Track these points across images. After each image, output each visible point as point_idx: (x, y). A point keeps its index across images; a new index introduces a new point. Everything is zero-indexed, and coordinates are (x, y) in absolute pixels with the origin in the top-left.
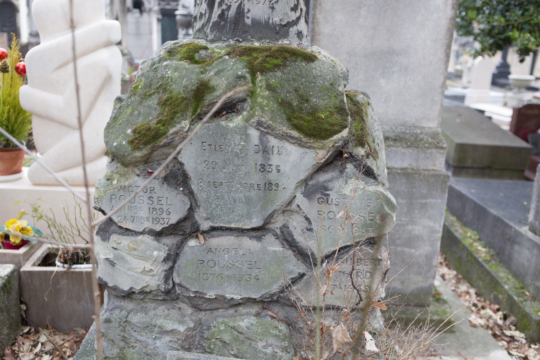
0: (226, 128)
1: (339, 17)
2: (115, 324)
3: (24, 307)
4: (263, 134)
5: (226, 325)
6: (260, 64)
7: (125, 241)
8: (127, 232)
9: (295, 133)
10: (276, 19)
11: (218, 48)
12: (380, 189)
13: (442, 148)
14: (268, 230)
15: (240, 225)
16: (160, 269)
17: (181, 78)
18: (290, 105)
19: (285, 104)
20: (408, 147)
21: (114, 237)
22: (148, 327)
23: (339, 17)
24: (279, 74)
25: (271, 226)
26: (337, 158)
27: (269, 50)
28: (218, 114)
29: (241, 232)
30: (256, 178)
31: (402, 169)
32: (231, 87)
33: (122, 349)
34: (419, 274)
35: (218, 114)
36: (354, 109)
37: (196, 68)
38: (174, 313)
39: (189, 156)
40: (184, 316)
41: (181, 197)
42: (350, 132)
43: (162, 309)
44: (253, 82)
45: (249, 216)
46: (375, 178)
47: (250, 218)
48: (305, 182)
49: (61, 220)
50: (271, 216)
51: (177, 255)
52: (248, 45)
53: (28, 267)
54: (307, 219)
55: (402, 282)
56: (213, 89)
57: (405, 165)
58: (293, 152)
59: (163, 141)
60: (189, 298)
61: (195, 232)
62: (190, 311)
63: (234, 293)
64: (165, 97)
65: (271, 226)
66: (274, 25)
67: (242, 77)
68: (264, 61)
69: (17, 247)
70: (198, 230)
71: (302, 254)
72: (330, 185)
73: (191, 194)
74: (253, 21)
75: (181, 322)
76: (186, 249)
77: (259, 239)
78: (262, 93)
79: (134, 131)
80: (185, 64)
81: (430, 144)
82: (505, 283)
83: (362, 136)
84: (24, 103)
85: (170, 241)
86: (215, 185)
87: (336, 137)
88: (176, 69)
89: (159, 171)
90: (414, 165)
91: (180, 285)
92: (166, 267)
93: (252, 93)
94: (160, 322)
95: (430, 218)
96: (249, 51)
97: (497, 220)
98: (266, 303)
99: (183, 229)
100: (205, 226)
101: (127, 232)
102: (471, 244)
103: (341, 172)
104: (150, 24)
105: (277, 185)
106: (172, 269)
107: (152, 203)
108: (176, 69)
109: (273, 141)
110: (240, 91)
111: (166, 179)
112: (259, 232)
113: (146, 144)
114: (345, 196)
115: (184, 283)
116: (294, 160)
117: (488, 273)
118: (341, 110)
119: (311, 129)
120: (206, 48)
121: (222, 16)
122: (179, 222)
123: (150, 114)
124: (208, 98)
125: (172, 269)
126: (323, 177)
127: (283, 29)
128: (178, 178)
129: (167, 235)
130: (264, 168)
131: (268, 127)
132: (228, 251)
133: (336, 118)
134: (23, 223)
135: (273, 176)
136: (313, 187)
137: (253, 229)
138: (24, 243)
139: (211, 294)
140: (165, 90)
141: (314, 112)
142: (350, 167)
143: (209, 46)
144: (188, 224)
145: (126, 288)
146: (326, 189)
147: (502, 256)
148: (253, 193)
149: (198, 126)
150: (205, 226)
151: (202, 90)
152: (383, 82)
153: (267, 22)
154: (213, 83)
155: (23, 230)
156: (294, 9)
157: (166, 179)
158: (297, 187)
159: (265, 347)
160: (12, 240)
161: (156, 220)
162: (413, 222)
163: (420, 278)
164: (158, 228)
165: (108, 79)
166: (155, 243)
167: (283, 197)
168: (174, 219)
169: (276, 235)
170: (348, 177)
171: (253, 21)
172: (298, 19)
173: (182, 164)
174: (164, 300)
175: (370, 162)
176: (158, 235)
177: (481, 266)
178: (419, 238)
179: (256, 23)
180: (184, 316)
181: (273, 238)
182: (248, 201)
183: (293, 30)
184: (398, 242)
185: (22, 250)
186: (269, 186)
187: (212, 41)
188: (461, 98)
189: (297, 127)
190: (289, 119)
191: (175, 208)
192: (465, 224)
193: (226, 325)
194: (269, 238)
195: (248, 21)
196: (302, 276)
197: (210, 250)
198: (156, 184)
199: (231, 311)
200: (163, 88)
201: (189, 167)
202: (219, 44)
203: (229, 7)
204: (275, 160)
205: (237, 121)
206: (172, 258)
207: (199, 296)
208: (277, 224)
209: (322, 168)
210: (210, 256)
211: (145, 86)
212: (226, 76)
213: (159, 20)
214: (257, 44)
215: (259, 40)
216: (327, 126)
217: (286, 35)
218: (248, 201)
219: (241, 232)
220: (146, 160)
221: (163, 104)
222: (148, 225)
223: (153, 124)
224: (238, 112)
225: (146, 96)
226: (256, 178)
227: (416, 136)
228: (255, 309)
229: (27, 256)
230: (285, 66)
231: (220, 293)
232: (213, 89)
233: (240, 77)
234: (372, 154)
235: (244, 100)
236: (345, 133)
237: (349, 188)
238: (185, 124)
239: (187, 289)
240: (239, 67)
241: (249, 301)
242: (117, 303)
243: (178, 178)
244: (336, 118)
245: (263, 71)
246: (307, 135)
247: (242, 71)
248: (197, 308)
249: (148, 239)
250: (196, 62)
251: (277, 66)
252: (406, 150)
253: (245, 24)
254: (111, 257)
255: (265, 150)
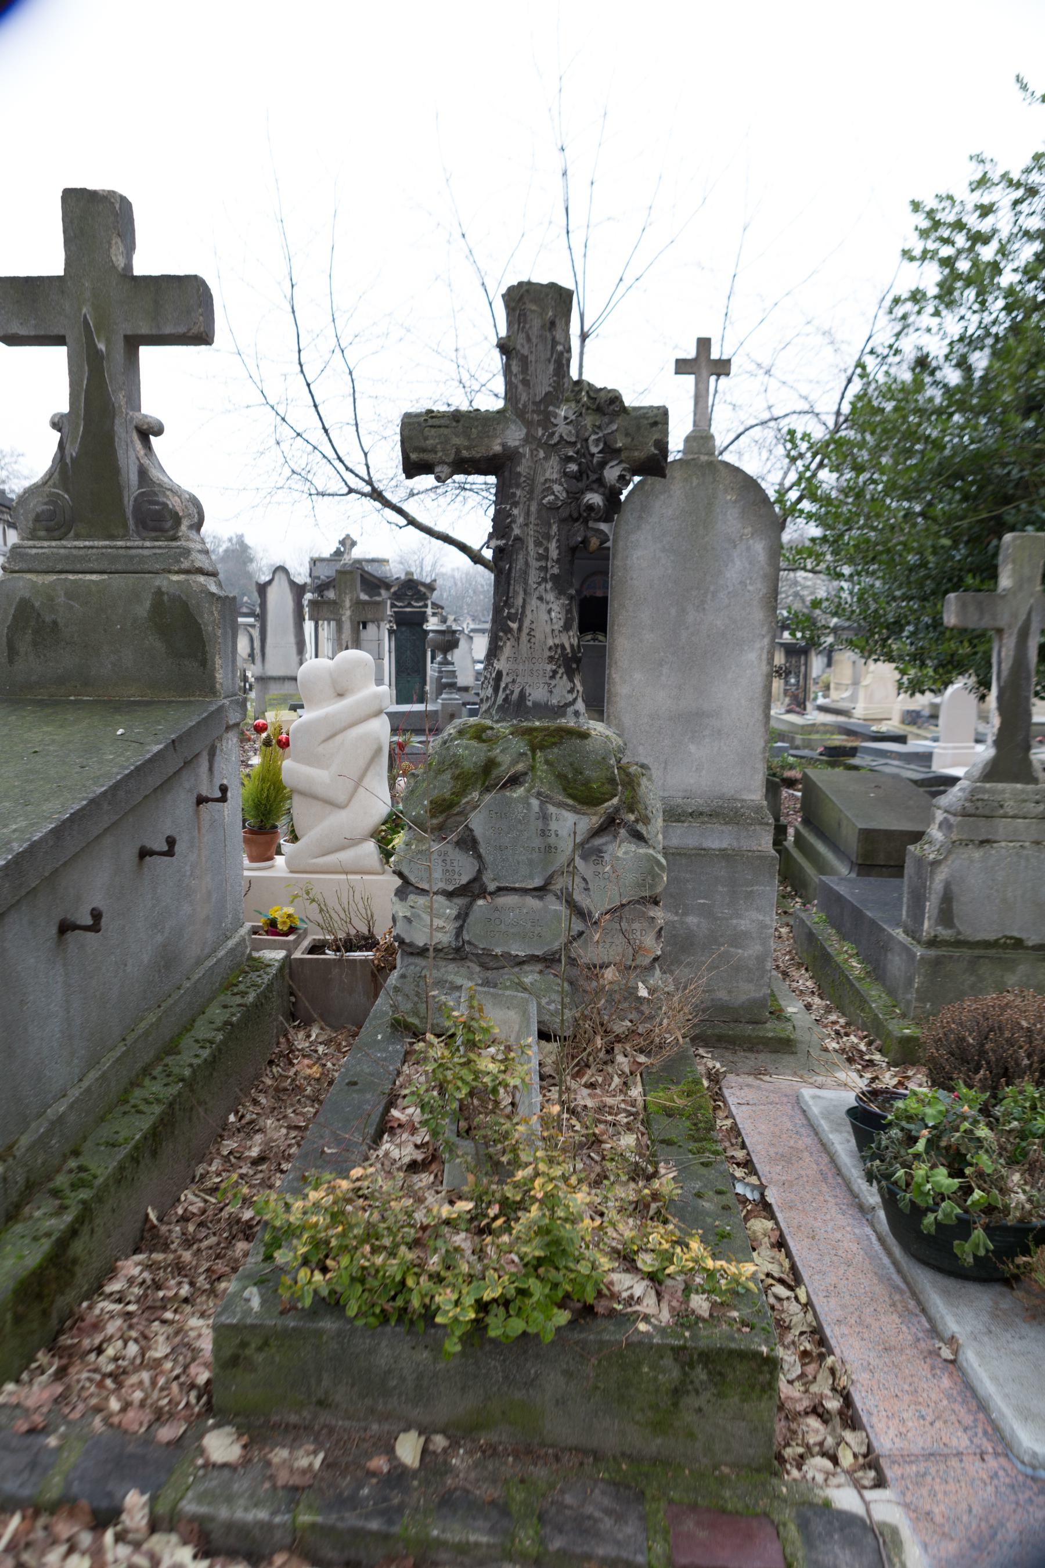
0: (511, 798)
1: (638, 676)
2: (410, 979)
3: (293, 999)
4: (542, 803)
5: (512, 981)
6: (539, 742)
7: (422, 901)
8: (423, 892)
9: (570, 802)
10: (554, 702)
11: (503, 728)
12: (651, 851)
13: (767, 824)
14: (550, 891)
15: (523, 885)
16: (451, 927)
17: (471, 755)
18: (566, 776)
19: (561, 777)
20: (726, 823)
21: (412, 897)
22: (439, 983)
23: (638, 676)
24: (556, 750)
25: (552, 887)
26: (609, 825)
27: (546, 729)
28: (504, 786)
29: (525, 891)
30: (537, 842)
31: (720, 850)
32: (514, 762)
33: (415, 1004)
34: (751, 981)
35: (504, 786)
36: (627, 779)
37: (484, 746)
38: (463, 970)
39: (478, 823)
40: (472, 973)
41: (471, 859)
42: (620, 800)
43: (452, 967)
44: (534, 759)
45: (531, 877)
46: (646, 842)
47: (533, 879)
48: (582, 844)
49: (332, 903)
50: (551, 877)
51: (467, 915)
52: (530, 724)
53: (297, 955)
54: (584, 879)
55: (729, 992)
56: (499, 765)
57: (724, 845)
58: (568, 819)
59: (457, 810)
60: (477, 955)
61: (483, 893)
62: (478, 969)
63: (519, 950)
64: (458, 772)
65: (552, 887)
66: (553, 707)
67: (524, 754)
68: (543, 740)
69: (286, 934)
70: (485, 891)
71: (581, 913)
72: (605, 848)
73: (479, 857)
74: (534, 703)
75: (470, 979)
76: (475, 907)
77: (541, 898)
78: (541, 767)
79: (431, 802)
80: (474, 743)
81: (752, 819)
82: (875, 1001)
83: (632, 804)
84: (285, 777)
85: (460, 901)
86: (501, 849)
87: (609, 803)
88: (466, 748)
89: (453, 837)
90: (735, 844)
91: (469, 943)
92: (457, 925)
93: (532, 768)
94: (450, 978)
95: (758, 910)
96: (530, 731)
97: (873, 923)
98: (549, 960)
99: (470, 891)
100: (492, 887)
101: (423, 892)
102: (846, 960)
103: (615, 837)
104: (380, 640)
105: (556, 848)
106: (461, 927)
107: (444, 865)
108: (466, 748)
109: (552, 809)
110: (520, 767)
111: (458, 844)
112: (541, 891)
113: (441, 812)
114: (618, 858)
115: (473, 941)
116: (569, 824)
117: (858, 992)
118: (612, 781)
119: (582, 794)
120: (492, 728)
121: (506, 700)
122: (469, 883)
123: (444, 786)
124: (495, 773)
125: (461, 927)
126: (598, 842)
127: (560, 710)
128: (468, 843)
129: (459, 896)
130: (544, 833)
131: (547, 796)
132: (513, 909)
133: (607, 788)
134: (290, 910)
135: (552, 840)
136: (589, 849)
137: (535, 889)
138: (292, 930)
139: (498, 951)
140: (457, 766)
141: (587, 783)
142: (623, 832)
143: (495, 726)
144: (476, 885)
145: (421, 944)
146: (601, 851)
147: (877, 971)
148: (535, 856)
149: (488, 797)
150: (492, 887)
151: (490, 765)
152: (692, 748)
153: (546, 704)
154: (499, 759)
155: (289, 916)
156: (571, 691)
157: (458, 844)
158: (574, 851)
159: (548, 1003)
160: (280, 927)
161: (449, 881)
162: (739, 916)
163: (751, 987)
164: (451, 888)
165: (379, 751)
166: (447, 903)
167: (562, 859)
168: (464, 880)
169: (556, 895)
170: (622, 842)
171: (534, 703)
172: (575, 700)
173: (471, 830)
174: (453, 959)
175: (640, 827)
176: (450, 895)
177: (853, 985)
178: (746, 934)
179: (536, 705)
180: (472, 973)
181: (554, 898)
182: (531, 862)
183: (570, 710)
184: (721, 940)
185: (291, 938)
186: (549, 849)
187: (497, 722)
188: (926, 758)
189: (571, 796)
190: (565, 790)
191: (464, 870)
192: (844, 937)
193: (512, 981)
194: (550, 898)
195: (529, 704)
196: (581, 934)
197: (496, 909)
198: (450, 848)
199: (516, 969)
200: (455, 763)
201: (478, 832)
202: (504, 724)
203: (512, 692)
204: (553, 826)
205: (520, 791)
206: (462, 916)
207: (488, 953)
208: (558, 885)
209: (598, 832)
210: (497, 914)
211: (439, 763)
212: (509, 755)
213: (391, 632)
214: (537, 723)
215: (539, 719)
216: (598, 795)
217: (563, 715)
218: (531, 862)
219: (525, 891)
220: (441, 828)
221: (456, 778)
222: (441, 885)
223: (447, 795)
224: (521, 784)
225: (440, 772)
226: (537, 842)
227: (736, 811)
228: (539, 967)
229: (297, 943)
230: (561, 743)
231: (506, 950)
232: (499, 765)
233: (522, 754)
234: (646, 820)
235: (526, 774)
236: (615, 801)
237: (622, 851)
238: (475, 795)
239: (476, 947)
240: (520, 745)
241: (533, 959)
242: (412, 959)
243: (468, 843)
244: (607, 788)
245: (542, 748)
246: (581, 802)
247: (524, 748)
248: (484, 967)
249: (440, 899)
250: (484, 741)
251: (554, 744)
252: (724, 827)
253: (526, 706)
254: (408, 914)
255: (545, 817)
